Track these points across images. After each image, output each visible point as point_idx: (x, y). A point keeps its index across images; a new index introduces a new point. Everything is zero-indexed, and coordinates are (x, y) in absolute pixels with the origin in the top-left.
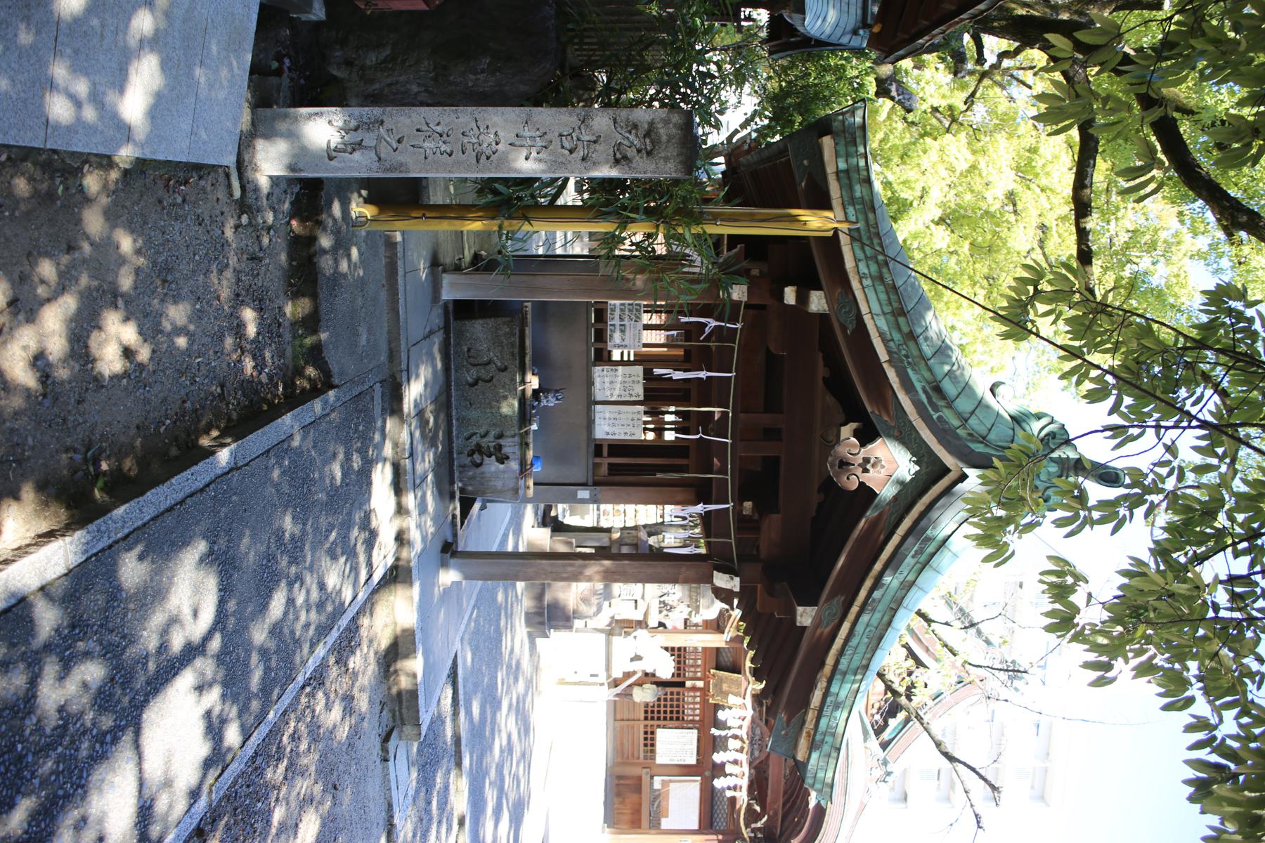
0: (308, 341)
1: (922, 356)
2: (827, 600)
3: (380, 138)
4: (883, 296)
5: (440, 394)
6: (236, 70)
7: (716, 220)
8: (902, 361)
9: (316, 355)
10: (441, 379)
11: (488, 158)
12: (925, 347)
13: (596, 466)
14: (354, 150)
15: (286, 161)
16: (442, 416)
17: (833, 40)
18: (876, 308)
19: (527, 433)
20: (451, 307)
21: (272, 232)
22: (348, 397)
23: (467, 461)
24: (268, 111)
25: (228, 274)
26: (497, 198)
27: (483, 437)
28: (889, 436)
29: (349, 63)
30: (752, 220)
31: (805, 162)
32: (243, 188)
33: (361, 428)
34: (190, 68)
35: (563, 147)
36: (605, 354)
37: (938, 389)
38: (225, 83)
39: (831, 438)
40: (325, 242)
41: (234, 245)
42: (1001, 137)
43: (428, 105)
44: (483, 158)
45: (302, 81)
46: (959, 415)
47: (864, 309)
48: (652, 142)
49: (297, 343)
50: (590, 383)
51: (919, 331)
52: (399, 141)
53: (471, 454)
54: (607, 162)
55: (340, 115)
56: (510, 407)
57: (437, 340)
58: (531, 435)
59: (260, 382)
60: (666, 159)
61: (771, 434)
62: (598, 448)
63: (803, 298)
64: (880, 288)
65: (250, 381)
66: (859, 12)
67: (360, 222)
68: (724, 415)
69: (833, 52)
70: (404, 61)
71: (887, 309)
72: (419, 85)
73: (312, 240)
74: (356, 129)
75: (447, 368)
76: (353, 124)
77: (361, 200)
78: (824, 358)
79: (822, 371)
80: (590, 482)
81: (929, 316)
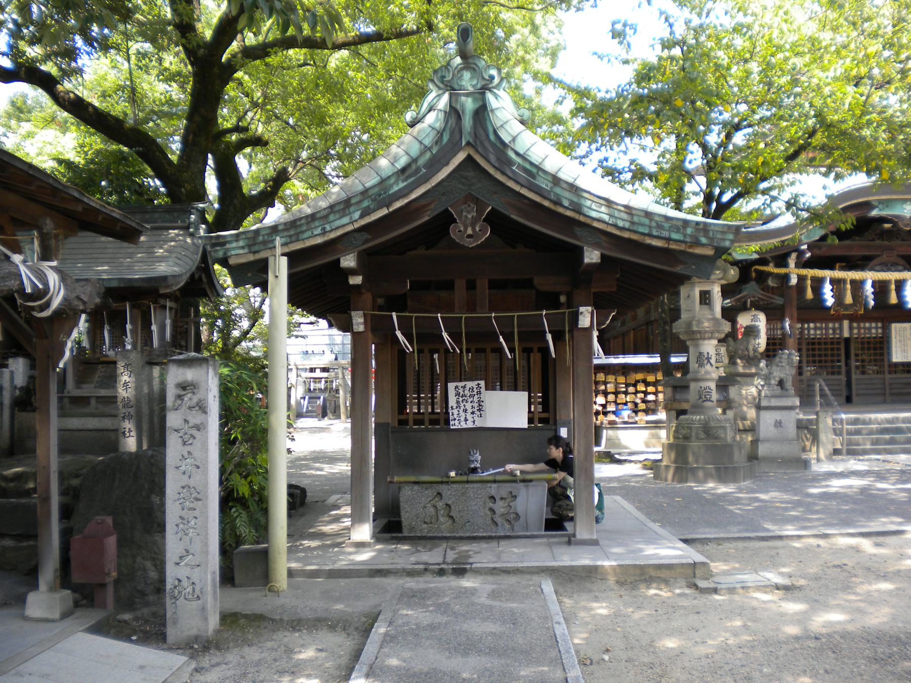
2: (578, 239)
18: (345, 220)
31: (249, 275)
37: (403, 170)
46: (422, 153)
47: (350, 228)
70: (155, 553)
79: (421, 251)
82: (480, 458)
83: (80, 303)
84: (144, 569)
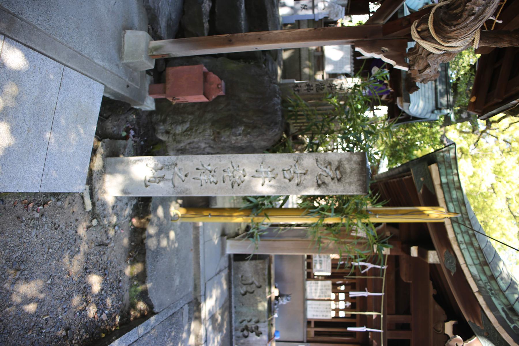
0: (140, 288)
1: (501, 290)
3: (174, 174)
4: (473, 254)
5: (225, 302)
6: (83, 135)
7: (376, 215)
8: (488, 292)
9: (144, 296)
10: (226, 293)
11: (239, 185)
12: (501, 283)
13: (308, 332)
14: (160, 181)
15: (121, 187)
16: (226, 314)
17: (422, 117)
19: (272, 319)
20: (232, 257)
21: (116, 228)
22: (164, 318)
23: (240, 334)
24: (113, 159)
25: (80, 257)
26: (251, 205)
27: (249, 322)
28: (481, 335)
29: (167, 132)
30: (397, 214)
31: (422, 179)
32: (93, 204)
33: (173, 334)
34: (40, 135)
35: (285, 178)
36: (312, 275)
37: (512, 309)
38: (74, 143)
39: (439, 329)
40: (152, 230)
41: (85, 239)
42: (487, 160)
43: (212, 154)
44: (236, 185)
45: (142, 143)
48: (341, 173)
49: (133, 289)
50: (304, 290)
51: (497, 274)
52: (186, 176)
53: (243, 331)
54: (312, 186)
55: (153, 161)
56: (263, 306)
57: (224, 275)
58: (274, 320)
59: (103, 321)
60: (350, 184)
61: (405, 327)
62: (309, 323)
63: (423, 254)
64: (472, 250)
65: (92, 321)
66: (434, 102)
67: (175, 218)
68: (379, 316)
69: (420, 123)
70: (196, 130)
71: (477, 262)
72: (206, 143)
73: (143, 230)
74: (161, 169)
75: (230, 288)
76: (160, 166)
77: (178, 205)
78: (433, 284)
79: (432, 291)
80: (305, 341)
81: (501, 264)
82: (284, 303)
83: (421, 68)
84: (183, 122)
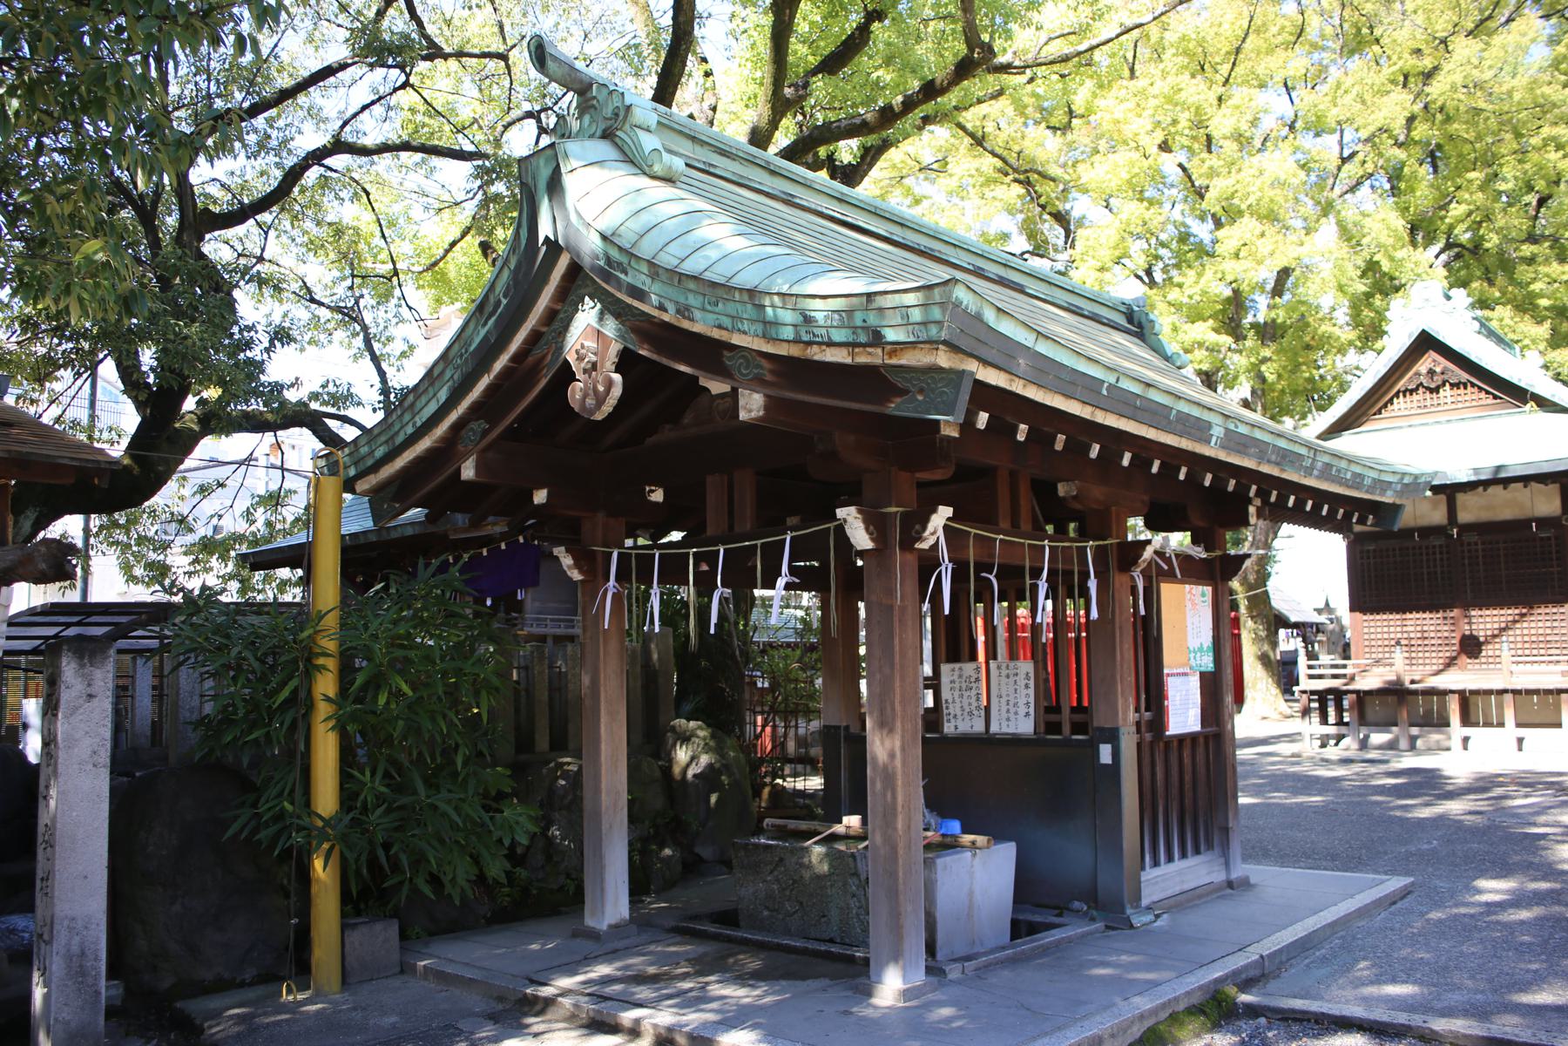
64: (419, 405)
